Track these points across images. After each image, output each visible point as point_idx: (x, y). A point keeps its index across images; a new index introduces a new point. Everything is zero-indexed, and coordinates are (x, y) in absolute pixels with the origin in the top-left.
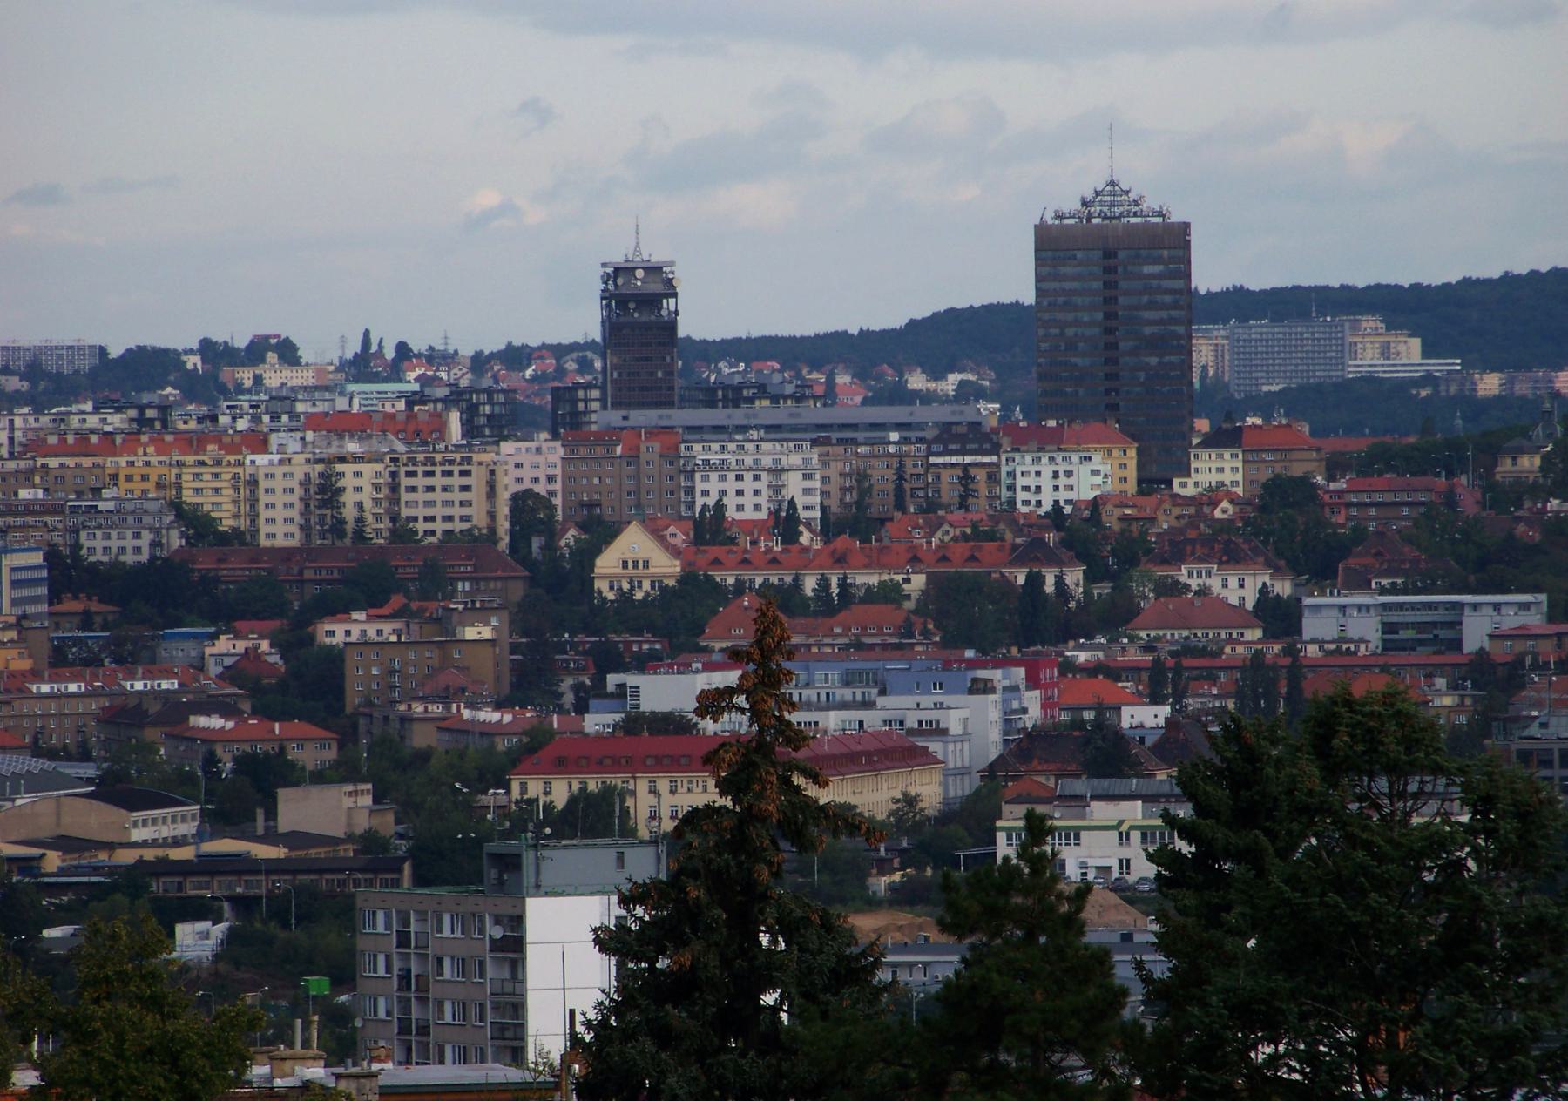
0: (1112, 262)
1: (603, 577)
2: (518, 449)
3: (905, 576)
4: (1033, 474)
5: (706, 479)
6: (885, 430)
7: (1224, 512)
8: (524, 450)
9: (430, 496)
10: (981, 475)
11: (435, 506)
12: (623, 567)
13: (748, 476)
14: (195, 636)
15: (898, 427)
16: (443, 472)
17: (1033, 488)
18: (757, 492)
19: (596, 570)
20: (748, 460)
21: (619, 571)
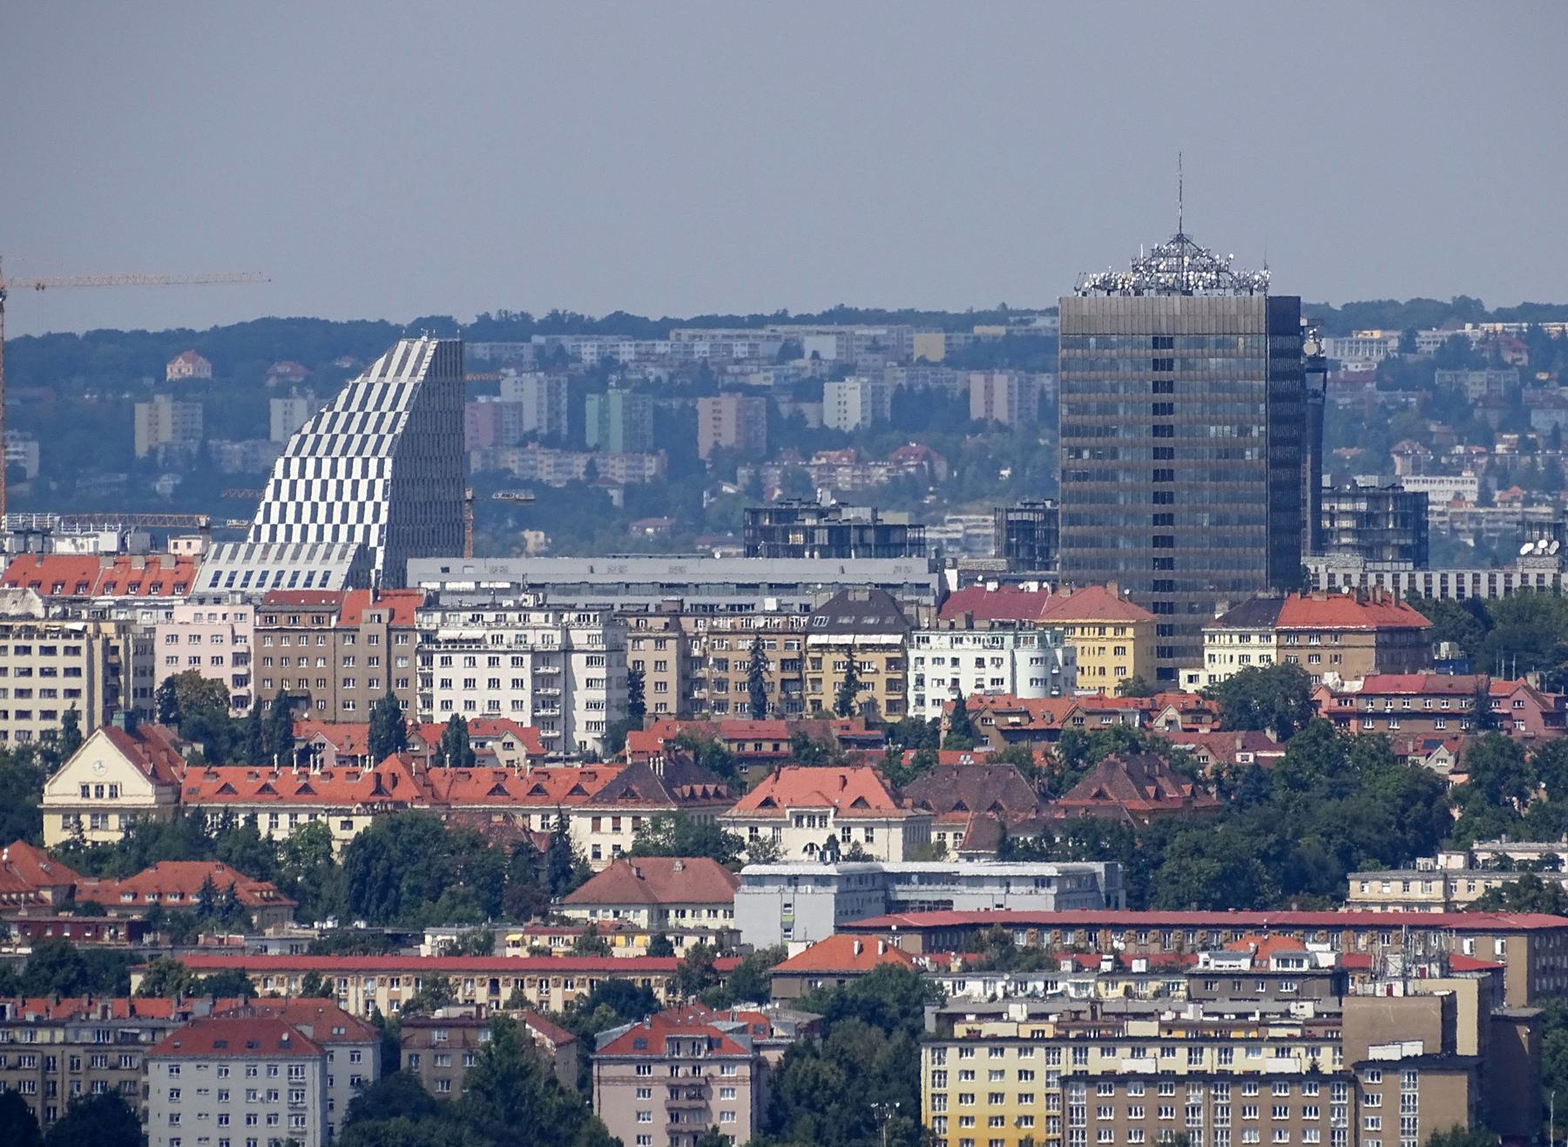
0: (1165, 353)
1: (53, 810)
2: (198, 616)
3: (345, 819)
4: (948, 662)
5: (446, 662)
6: (756, 594)
7: (1169, 722)
8: (205, 616)
9: (24, 683)
10: (878, 660)
11: (66, 691)
12: (83, 795)
13: (505, 660)
14: (1284, 928)
15: (775, 588)
16: (41, 648)
17: (948, 682)
18: (517, 683)
19: (46, 800)
20: (509, 636)
21: (78, 800)
